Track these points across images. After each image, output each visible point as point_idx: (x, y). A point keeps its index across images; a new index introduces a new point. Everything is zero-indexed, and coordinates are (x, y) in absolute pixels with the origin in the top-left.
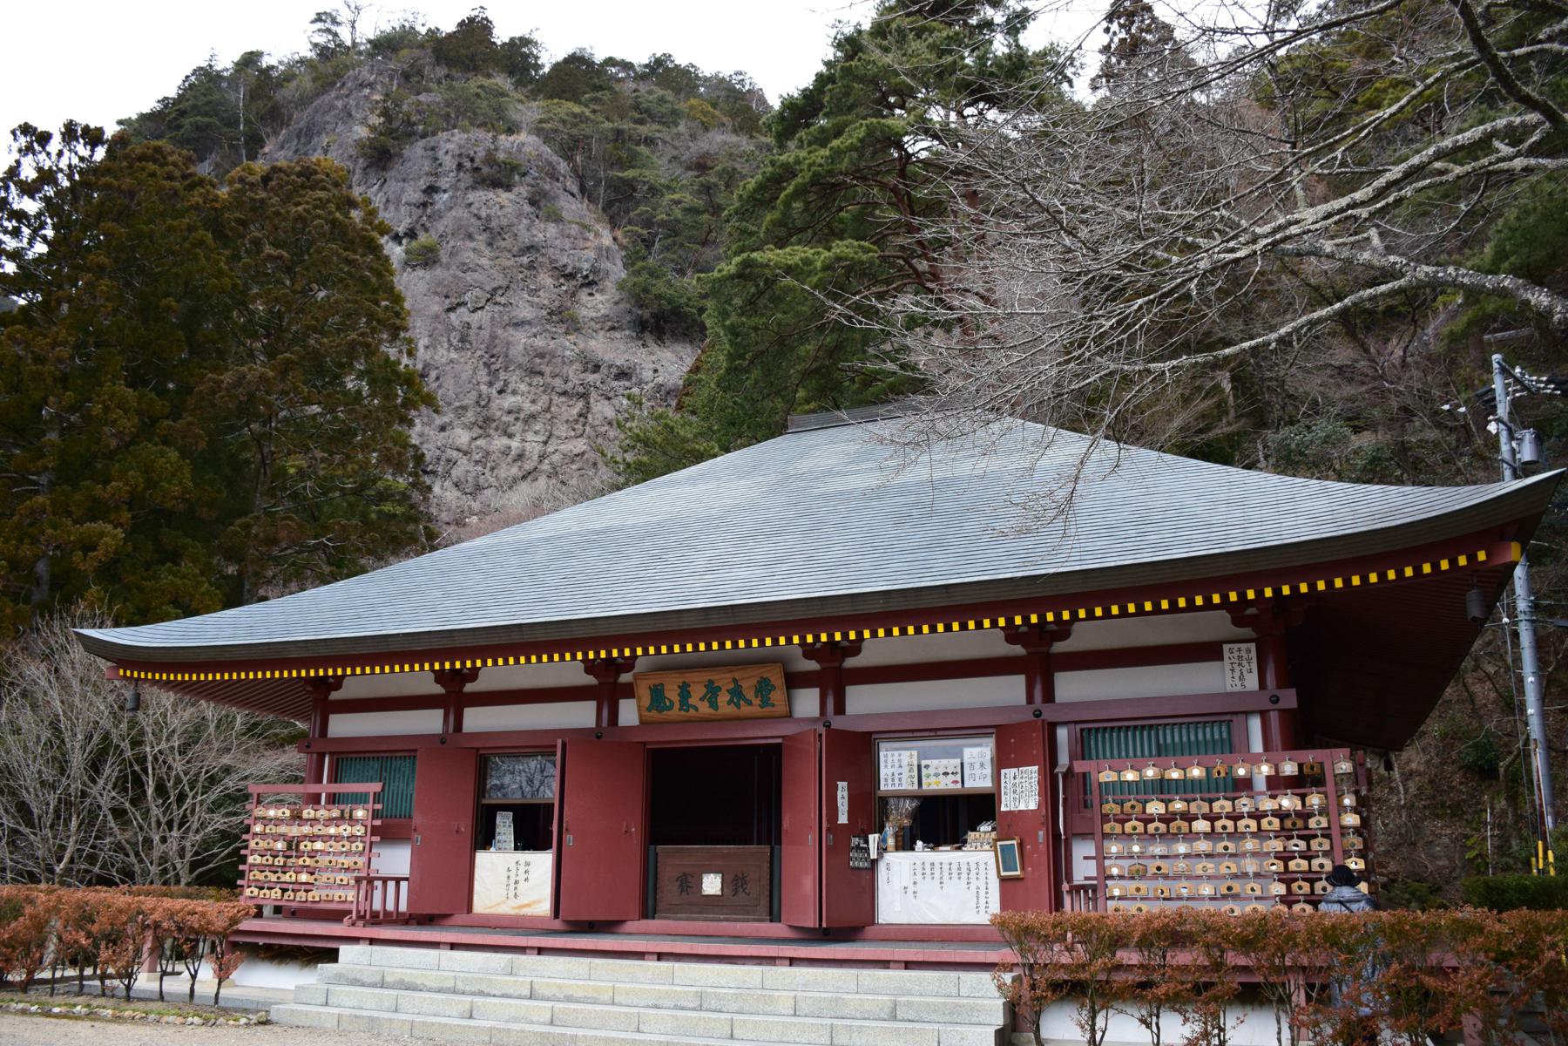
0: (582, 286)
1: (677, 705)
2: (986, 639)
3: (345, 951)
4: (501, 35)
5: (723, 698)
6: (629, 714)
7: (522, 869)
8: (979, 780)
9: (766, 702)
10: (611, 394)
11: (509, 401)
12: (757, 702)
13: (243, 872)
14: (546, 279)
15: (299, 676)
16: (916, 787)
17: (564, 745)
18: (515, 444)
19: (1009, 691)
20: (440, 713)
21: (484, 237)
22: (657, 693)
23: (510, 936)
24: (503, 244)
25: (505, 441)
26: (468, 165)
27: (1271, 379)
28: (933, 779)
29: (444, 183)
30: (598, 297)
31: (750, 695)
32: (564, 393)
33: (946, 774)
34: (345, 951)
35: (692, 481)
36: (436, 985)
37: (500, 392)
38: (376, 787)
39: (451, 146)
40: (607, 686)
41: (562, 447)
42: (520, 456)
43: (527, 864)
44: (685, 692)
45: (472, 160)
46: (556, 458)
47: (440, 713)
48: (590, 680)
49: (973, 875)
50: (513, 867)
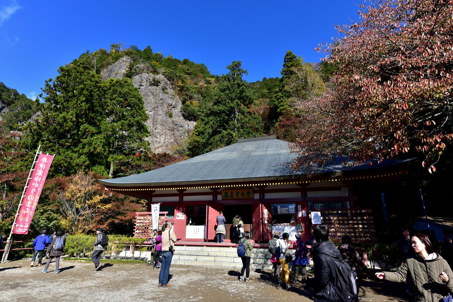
2: (174, 190)
5: (240, 195)
6: (220, 197)
8: (293, 211)
9: (238, 196)
11: (157, 131)
12: (247, 196)
18: (158, 140)
19: (298, 195)
20: (178, 197)
21: (152, 96)
22: (226, 193)
23: (193, 243)
25: (156, 139)
27: (97, 91)
30: (176, 110)
31: (245, 194)
35: (222, 152)
36: (186, 254)
39: (145, 76)
42: (159, 142)
44: (232, 194)
46: (167, 143)
47: (178, 197)
48: (178, 192)
50: (195, 229)
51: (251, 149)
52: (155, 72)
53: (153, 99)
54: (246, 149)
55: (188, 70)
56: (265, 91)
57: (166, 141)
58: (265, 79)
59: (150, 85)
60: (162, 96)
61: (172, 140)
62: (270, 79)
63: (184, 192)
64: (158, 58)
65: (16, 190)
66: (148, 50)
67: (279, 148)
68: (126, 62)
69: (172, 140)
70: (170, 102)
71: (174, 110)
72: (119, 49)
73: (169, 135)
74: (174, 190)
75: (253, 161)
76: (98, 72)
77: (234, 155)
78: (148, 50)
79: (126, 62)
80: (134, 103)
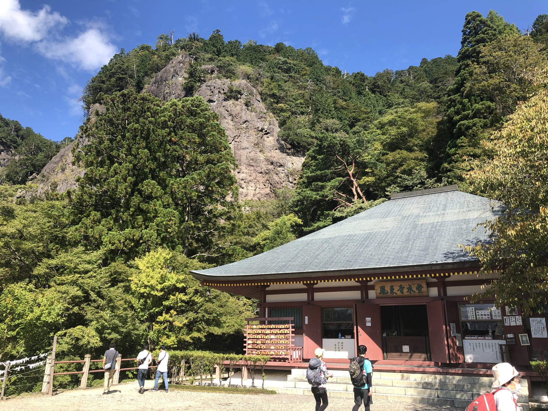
0: (265, 134)
1: (389, 292)
2: (300, 285)
3: (293, 370)
4: (226, 40)
5: (405, 291)
6: (372, 294)
7: (340, 344)
10: (278, 173)
12: (417, 291)
13: (246, 346)
14: (252, 132)
15: (261, 285)
16: (475, 319)
17: (356, 305)
20: (306, 294)
22: (383, 288)
24: (237, 120)
26: (222, 92)
28: (480, 316)
29: (215, 98)
31: (414, 289)
32: (261, 173)
33: (485, 315)
34: (293, 370)
35: (370, 217)
37: (238, 173)
38: (292, 318)
40: (364, 288)
41: (261, 191)
43: (342, 343)
44: (392, 288)
45: (223, 90)
46: (258, 195)
47: (306, 294)
49: (494, 347)
50: (337, 344)
51: (416, 212)
52: (230, 74)
53: (231, 123)
54: (406, 213)
55: (285, 63)
56: (425, 84)
57: (257, 192)
58: (424, 61)
59: (225, 100)
60: (246, 115)
61: (268, 190)
62: (434, 61)
63: (267, 289)
64: (234, 49)
65: (91, 301)
66: (216, 38)
67: (465, 209)
68: (183, 62)
69: (268, 190)
70: (260, 125)
71: (266, 139)
72: (170, 42)
73: (261, 181)
74: (300, 285)
75: (423, 234)
76: (139, 87)
77: (389, 224)
78: (216, 38)
79: (183, 62)
80: (210, 142)
